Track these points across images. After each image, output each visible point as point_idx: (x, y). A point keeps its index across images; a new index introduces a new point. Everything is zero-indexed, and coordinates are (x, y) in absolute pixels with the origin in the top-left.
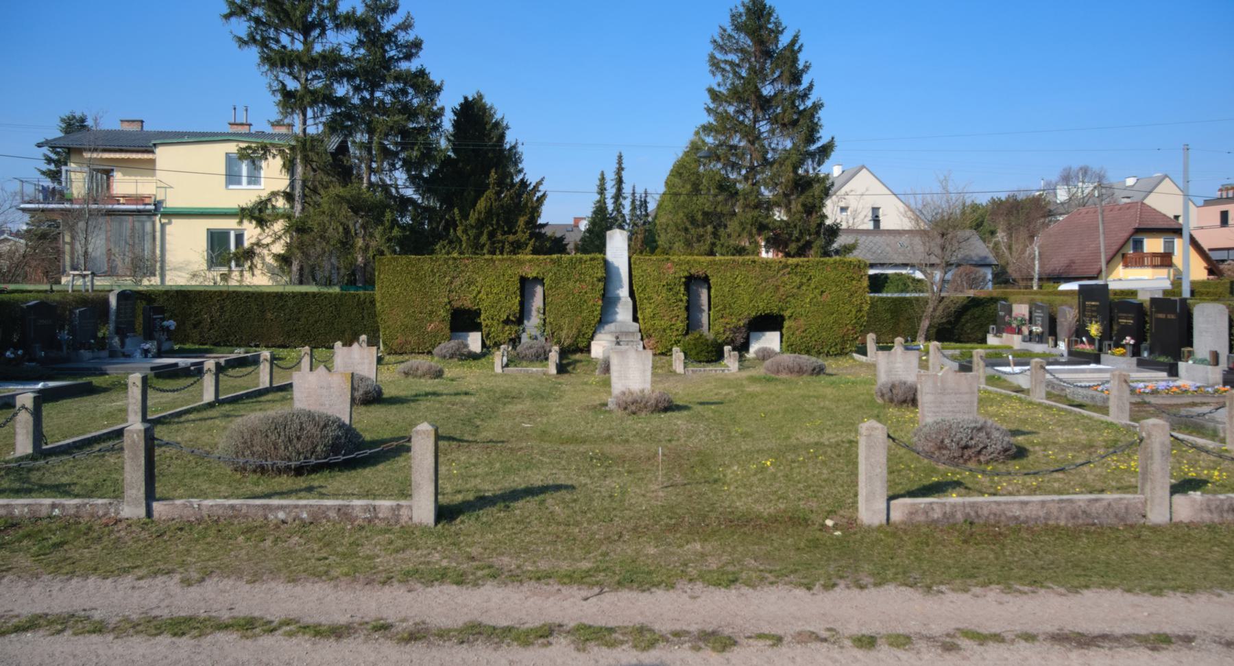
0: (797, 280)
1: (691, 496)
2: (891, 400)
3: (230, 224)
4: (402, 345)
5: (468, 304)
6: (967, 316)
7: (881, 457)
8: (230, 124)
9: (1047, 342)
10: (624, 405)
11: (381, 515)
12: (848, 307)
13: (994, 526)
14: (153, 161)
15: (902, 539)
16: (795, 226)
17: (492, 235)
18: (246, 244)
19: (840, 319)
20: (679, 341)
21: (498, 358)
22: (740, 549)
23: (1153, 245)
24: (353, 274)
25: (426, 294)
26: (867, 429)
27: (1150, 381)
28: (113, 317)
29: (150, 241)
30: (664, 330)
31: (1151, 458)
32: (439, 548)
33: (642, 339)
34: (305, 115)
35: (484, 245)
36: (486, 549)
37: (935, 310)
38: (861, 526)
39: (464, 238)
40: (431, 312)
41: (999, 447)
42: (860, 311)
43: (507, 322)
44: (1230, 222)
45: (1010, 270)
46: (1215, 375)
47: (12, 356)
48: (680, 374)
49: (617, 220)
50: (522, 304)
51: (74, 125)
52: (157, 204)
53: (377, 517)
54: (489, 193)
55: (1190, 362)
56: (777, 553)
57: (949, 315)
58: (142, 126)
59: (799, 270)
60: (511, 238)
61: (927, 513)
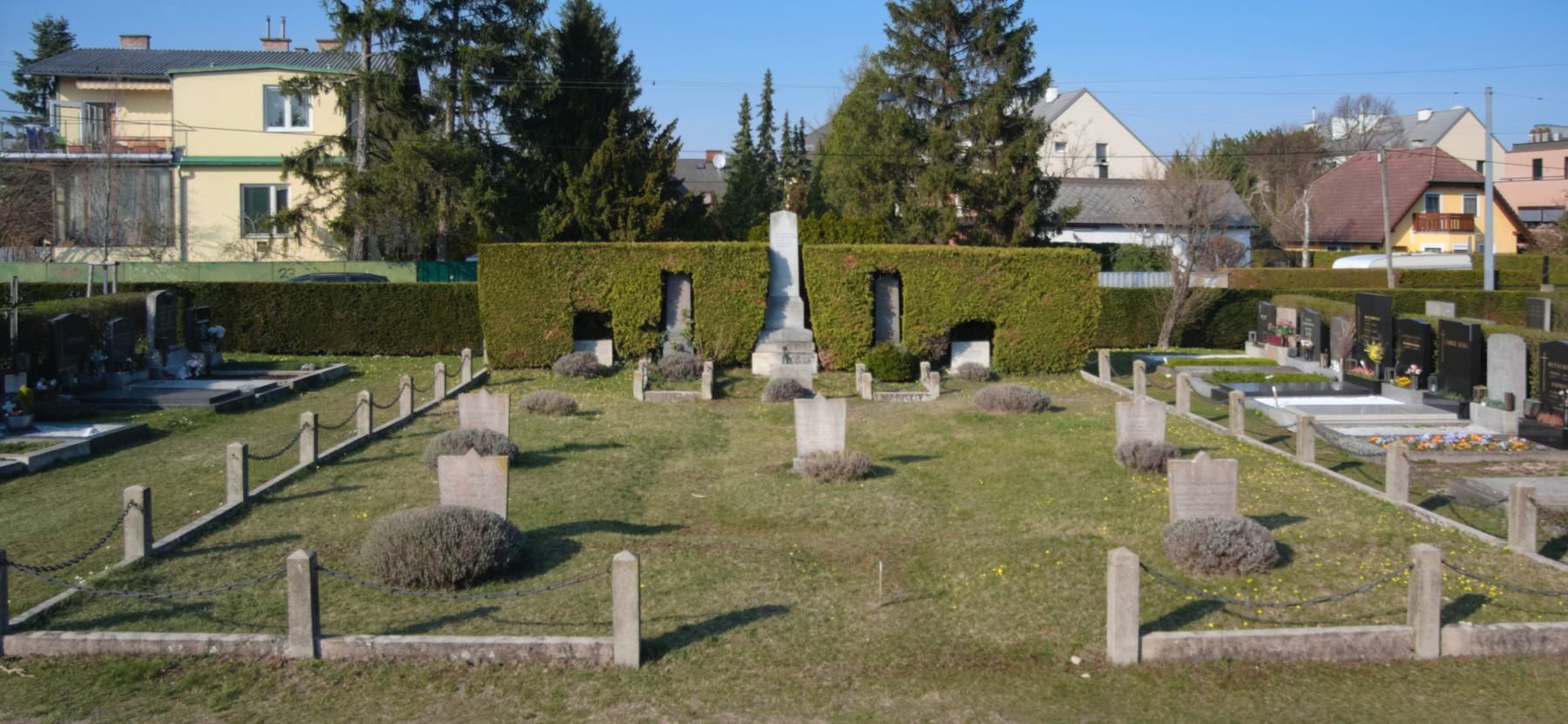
0: (1011, 278)
1: (917, 620)
2: (1134, 466)
3: (271, 178)
4: (512, 358)
5: (595, 305)
6: (1221, 314)
7: (1133, 590)
8: (264, 40)
9: (1318, 360)
10: (815, 471)
11: (578, 655)
12: (1075, 313)
13: (1254, 664)
14: (169, 94)
15: (1155, 684)
16: (1002, 184)
17: (612, 197)
18: (292, 205)
19: (1065, 327)
20: (863, 354)
21: (638, 375)
22: (982, 699)
23: (1451, 203)
24: (434, 245)
25: (542, 292)
26: (1118, 559)
27: (1437, 425)
28: (152, 327)
29: (167, 199)
30: (845, 340)
31: (1422, 588)
32: (653, 700)
33: (817, 351)
34: (368, 40)
35: (602, 210)
36: (705, 701)
37: (1181, 306)
38: (1110, 665)
39: (577, 201)
40: (549, 316)
41: (1260, 555)
42: (1089, 317)
43: (645, 328)
44: (1545, 173)
45: (1274, 231)
46: (1510, 421)
47: (45, 388)
48: (866, 400)
49: (765, 159)
50: (664, 305)
51: (54, 39)
52: (176, 152)
53: (574, 657)
54: (608, 143)
55: (1483, 404)
56: (1022, 703)
57: (1198, 314)
58: (148, 44)
59: (1013, 265)
60: (637, 200)
61: (1182, 649)
